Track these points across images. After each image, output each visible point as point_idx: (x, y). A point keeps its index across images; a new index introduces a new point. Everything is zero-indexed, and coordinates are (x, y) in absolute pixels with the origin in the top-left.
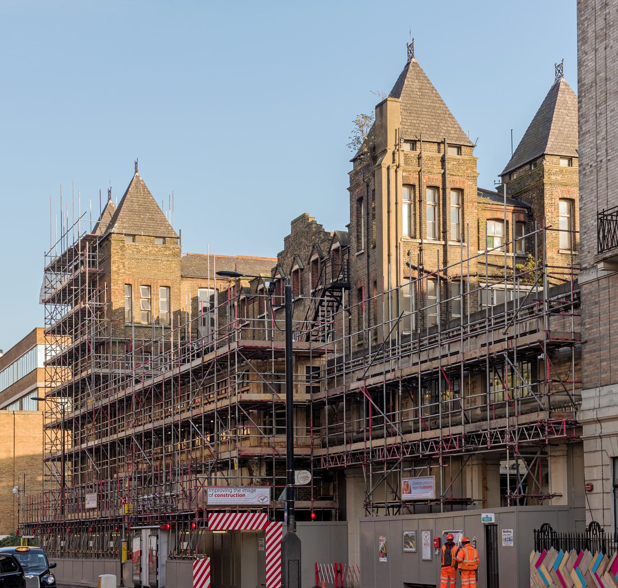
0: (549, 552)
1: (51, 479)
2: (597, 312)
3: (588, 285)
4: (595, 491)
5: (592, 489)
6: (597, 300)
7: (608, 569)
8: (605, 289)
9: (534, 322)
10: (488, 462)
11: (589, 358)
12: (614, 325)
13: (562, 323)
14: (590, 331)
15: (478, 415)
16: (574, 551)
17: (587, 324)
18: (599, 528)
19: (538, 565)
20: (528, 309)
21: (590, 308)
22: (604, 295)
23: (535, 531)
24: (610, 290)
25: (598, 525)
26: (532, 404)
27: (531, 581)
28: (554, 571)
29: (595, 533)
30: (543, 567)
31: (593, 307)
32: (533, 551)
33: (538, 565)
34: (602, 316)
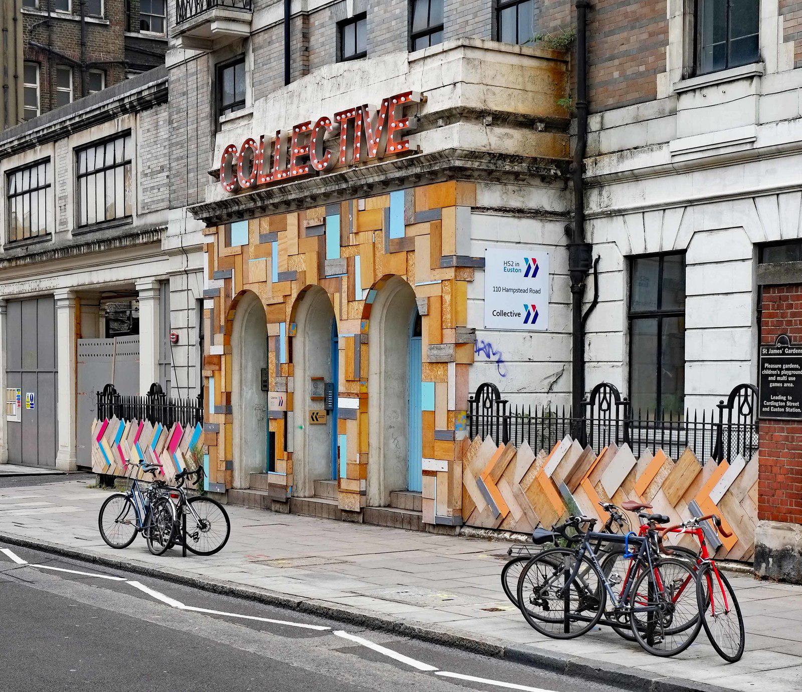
0: (111, 422)
1: (120, 242)
2: (185, 105)
3: (175, 69)
4: (180, 343)
5: (177, 341)
6: (185, 90)
7: (166, 446)
8: (192, 74)
9: (126, 118)
10: (83, 302)
11: (177, 167)
12: (202, 123)
13: (155, 121)
14: (178, 132)
15: (70, 241)
16: (135, 421)
17: (174, 121)
18: (498, 396)
19: (99, 438)
20: (119, 100)
21: (178, 100)
22: (192, 81)
23: (98, 394)
24: (199, 76)
25: (496, 391)
26: (127, 227)
27: (93, 458)
28: (115, 446)
29: (488, 405)
30: (104, 441)
31: (181, 99)
32: (95, 420)
33: (99, 438)
34: (189, 112)
